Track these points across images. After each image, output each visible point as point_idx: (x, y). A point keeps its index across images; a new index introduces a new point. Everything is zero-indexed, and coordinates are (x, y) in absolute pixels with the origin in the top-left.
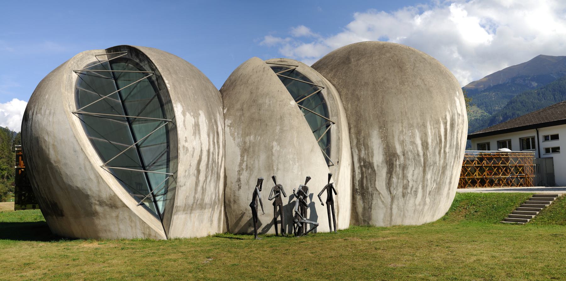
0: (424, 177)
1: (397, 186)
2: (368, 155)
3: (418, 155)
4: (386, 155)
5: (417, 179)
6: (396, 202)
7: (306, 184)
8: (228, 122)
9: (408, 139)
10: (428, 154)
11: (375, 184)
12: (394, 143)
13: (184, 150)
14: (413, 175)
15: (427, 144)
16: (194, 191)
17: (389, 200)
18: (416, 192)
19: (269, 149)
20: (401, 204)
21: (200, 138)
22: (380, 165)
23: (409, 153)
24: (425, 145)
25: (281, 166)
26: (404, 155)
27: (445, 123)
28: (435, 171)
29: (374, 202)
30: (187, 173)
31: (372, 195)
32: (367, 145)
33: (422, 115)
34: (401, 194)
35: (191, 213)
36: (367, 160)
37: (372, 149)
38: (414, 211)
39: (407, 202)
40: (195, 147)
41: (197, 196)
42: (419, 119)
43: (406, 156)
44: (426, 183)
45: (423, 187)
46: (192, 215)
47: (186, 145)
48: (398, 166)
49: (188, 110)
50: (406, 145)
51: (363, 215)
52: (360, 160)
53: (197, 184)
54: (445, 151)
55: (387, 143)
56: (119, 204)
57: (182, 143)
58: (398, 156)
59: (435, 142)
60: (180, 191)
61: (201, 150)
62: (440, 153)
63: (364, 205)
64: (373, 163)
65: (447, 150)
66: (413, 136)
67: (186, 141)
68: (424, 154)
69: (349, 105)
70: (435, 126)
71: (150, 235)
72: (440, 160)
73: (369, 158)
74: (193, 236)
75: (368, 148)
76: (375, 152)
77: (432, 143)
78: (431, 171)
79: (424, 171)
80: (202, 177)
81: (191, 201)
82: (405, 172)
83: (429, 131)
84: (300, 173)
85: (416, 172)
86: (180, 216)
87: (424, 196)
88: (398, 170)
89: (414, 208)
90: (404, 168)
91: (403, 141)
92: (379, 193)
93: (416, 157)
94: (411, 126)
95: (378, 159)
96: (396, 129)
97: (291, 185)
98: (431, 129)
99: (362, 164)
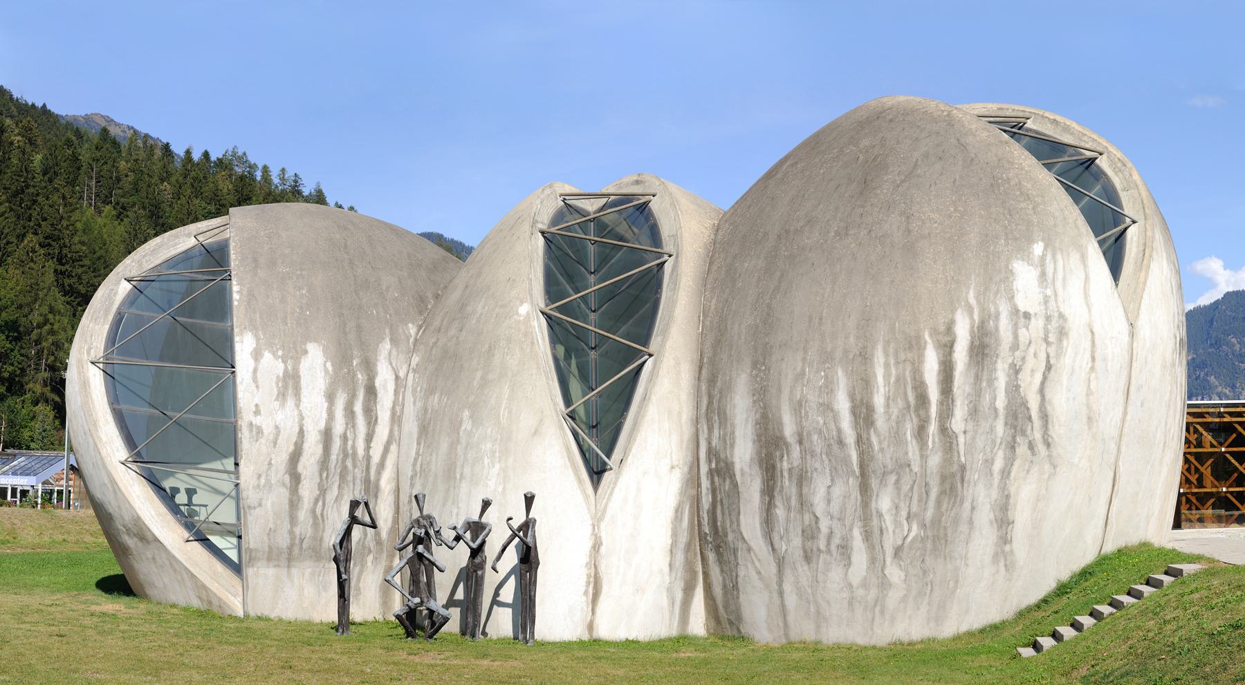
0: (865, 504)
1: (786, 530)
2: (725, 441)
3: (841, 442)
4: (760, 441)
5: (843, 510)
6: (788, 573)
7: (421, 510)
8: (416, 360)
9: (813, 398)
10: (874, 439)
11: (738, 525)
12: (779, 409)
13: (251, 431)
14: (829, 501)
15: (870, 409)
16: (287, 519)
17: (773, 569)
18: (845, 549)
19: (456, 426)
20: (804, 582)
21: (298, 406)
22: (747, 469)
23: (815, 437)
24: (863, 414)
25: (467, 470)
26: (800, 442)
27: (947, 349)
28: (905, 488)
29: (742, 573)
30: (263, 481)
31: (735, 551)
32: (725, 413)
33: (867, 322)
34: (799, 554)
35: (289, 567)
36: (722, 456)
37: (733, 425)
38: (850, 604)
39: (821, 577)
40: (282, 426)
41: (297, 531)
42: (852, 339)
43: (806, 444)
44: (875, 522)
45: (867, 536)
46: (294, 571)
47: (257, 421)
48: (786, 474)
49: (271, 346)
50: (806, 413)
51: (726, 607)
52: (710, 450)
53: (294, 503)
54: (944, 430)
55: (765, 408)
56: (150, 538)
57: (246, 417)
58: (787, 445)
59: (901, 403)
60: (250, 518)
61: (301, 432)
62: (921, 432)
63: (724, 580)
64: (733, 463)
65: (958, 423)
66: (829, 387)
67: (257, 412)
68: (859, 440)
69: (714, 301)
70: (902, 356)
71: (210, 603)
72: (924, 457)
73: (725, 448)
74: (301, 616)
75: (726, 419)
76: (737, 433)
77: (887, 406)
78: (890, 488)
79: (865, 488)
80: (308, 490)
81: (283, 541)
82: (805, 490)
83: (880, 373)
84: (500, 489)
85: (837, 491)
86: (262, 571)
87: (875, 561)
88: (787, 484)
89: (846, 595)
90: (802, 478)
91: (800, 403)
92: (749, 550)
93: (835, 447)
94: (827, 358)
95: (743, 453)
96: (788, 366)
97: (451, 515)
98: (887, 365)
99: (713, 465)
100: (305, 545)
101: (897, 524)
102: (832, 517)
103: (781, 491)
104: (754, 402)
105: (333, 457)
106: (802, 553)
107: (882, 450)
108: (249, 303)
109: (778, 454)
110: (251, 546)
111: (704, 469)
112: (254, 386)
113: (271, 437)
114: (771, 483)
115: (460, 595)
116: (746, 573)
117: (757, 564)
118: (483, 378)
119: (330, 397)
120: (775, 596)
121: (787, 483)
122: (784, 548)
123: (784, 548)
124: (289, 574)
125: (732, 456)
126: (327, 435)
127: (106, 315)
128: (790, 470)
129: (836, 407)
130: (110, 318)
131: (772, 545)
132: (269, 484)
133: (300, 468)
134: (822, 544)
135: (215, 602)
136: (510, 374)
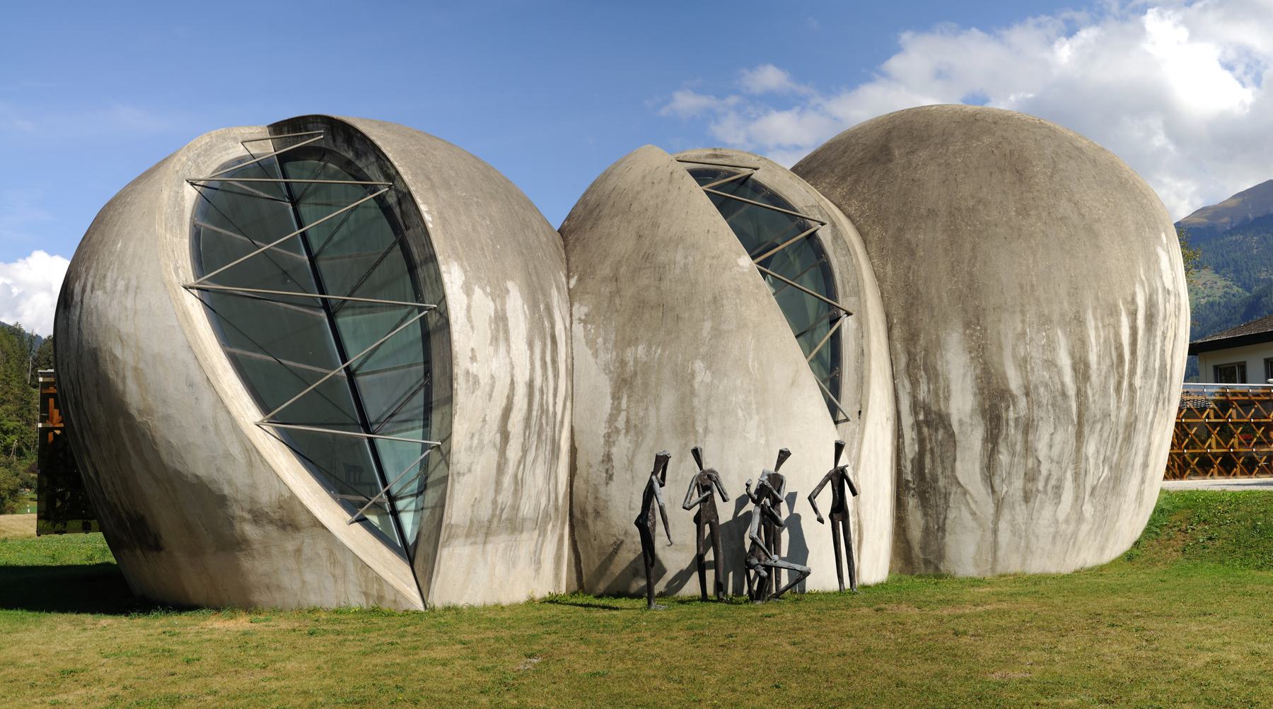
1: (1009, 474)
2: (937, 395)
3: (1064, 394)
5: (1061, 454)
6: (1006, 515)
7: (777, 468)
9: (1037, 355)
10: (1090, 392)
13: (468, 381)
14: (1051, 447)
15: (1087, 366)
16: (493, 486)
17: (991, 509)
18: (1058, 489)
19: (684, 380)
20: (1020, 519)
21: (508, 352)
23: (1042, 390)
24: (1081, 369)
25: (714, 423)
26: (1027, 395)
27: (1133, 314)
28: (1105, 435)
29: (952, 515)
30: (476, 441)
31: (946, 496)
32: (935, 368)
35: (485, 543)
37: (947, 379)
38: (1054, 537)
39: (1035, 516)
41: (500, 499)
43: (1033, 396)
44: (1083, 465)
45: (1076, 477)
46: (489, 547)
47: (474, 368)
48: (1012, 423)
49: (479, 279)
50: (1032, 369)
51: (924, 548)
53: (501, 469)
55: (985, 363)
56: (303, 519)
57: (462, 364)
58: (1012, 396)
59: (1108, 362)
60: (457, 486)
61: (512, 383)
62: (1118, 389)
63: (927, 522)
64: (948, 415)
65: (1138, 382)
66: (1051, 346)
71: (381, 598)
75: (937, 376)
77: (1099, 363)
78: (1096, 435)
79: (1079, 435)
80: (513, 452)
81: (485, 512)
82: (1031, 437)
83: (1092, 333)
84: (762, 441)
85: (1058, 438)
86: (457, 551)
88: (1013, 433)
89: (1052, 530)
90: (1028, 427)
91: (1025, 360)
92: (965, 493)
93: (1059, 398)
94: (1045, 321)
95: (961, 404)
96: (1008, 329)
98: (1097, 328)
99: (921, 417)
100: (504, 516)
101: (1097, 465)
102: (1052, 461)
103: (1006, 438)
104: (972, 358)
105: (534, 413)
106: (1022, 494)
107: (1094, 401)
108: (444, 226)
109: (1003, 405)
110: (453, 522)
111: (907, 421)
112: (469, 328)
113: (487, 389)
114: (995, 432)
115: (710, 556)
116: (958, 515)
117: (973, 506)
118: (714, 329)
119: (531, 345)
120: (989, 535)
121: (1013, 431)
122: (1005, 489)
123: (1005, 489)
124: (484, 551)
125: (947, 408)
126: (531, 385)
127: (181, 225)
128: (1016, 420)
129: (1059, 363)
130: (187, 229)
131: (992, 487)
132: (481, 445)
133: (510, 427)
134: (1041, 485)
135: (389, 596)
136: (751, 325)
